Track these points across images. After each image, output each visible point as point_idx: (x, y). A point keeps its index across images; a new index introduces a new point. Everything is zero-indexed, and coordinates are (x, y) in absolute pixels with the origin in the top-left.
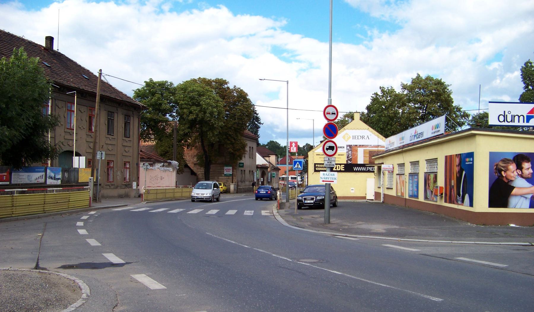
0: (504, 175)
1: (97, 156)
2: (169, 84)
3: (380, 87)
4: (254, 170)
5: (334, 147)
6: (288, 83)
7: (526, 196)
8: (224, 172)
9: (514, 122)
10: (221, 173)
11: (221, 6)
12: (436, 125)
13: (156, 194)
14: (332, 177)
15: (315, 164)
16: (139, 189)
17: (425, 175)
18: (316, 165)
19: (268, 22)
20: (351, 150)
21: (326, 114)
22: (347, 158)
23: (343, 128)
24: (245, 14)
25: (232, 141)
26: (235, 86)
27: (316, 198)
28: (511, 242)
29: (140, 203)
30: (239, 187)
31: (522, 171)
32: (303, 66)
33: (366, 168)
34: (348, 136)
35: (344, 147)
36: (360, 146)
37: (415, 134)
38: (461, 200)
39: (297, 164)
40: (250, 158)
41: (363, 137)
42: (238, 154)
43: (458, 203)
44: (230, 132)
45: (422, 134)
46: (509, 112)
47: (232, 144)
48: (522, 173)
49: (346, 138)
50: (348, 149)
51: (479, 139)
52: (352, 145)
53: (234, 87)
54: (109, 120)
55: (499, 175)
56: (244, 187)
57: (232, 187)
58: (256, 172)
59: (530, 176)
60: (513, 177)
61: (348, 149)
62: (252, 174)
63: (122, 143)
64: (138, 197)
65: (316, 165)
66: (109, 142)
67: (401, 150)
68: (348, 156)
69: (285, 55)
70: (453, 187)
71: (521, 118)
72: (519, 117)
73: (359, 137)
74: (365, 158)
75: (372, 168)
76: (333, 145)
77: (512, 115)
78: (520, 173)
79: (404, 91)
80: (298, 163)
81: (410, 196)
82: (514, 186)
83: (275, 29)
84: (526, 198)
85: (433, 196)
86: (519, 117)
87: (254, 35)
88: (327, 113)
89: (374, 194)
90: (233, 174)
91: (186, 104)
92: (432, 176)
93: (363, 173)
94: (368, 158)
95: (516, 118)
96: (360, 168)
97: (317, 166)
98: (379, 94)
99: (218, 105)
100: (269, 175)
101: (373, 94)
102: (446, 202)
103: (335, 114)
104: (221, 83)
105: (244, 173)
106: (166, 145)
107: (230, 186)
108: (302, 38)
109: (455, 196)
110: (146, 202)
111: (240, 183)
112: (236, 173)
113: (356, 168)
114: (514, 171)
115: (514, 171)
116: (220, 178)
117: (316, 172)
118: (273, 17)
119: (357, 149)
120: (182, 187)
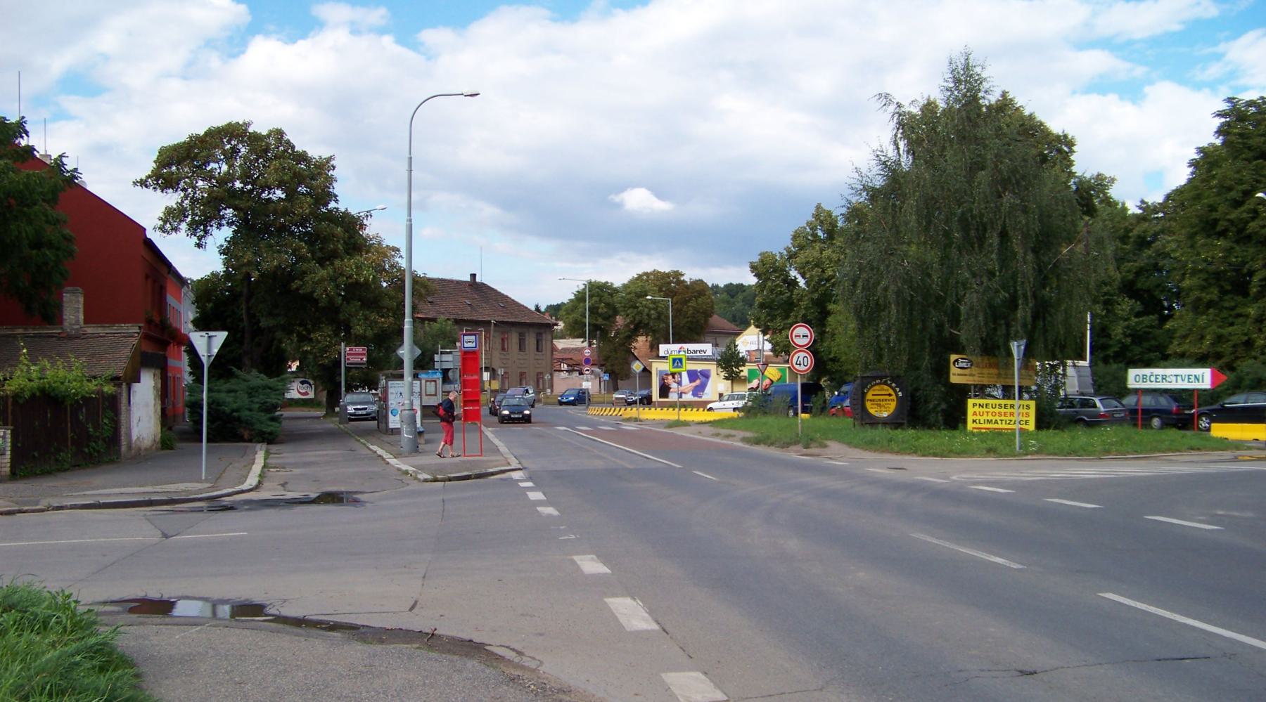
21: (794, 337)
54: (520, 339)
66: (521, 357)
88: (796, 336)
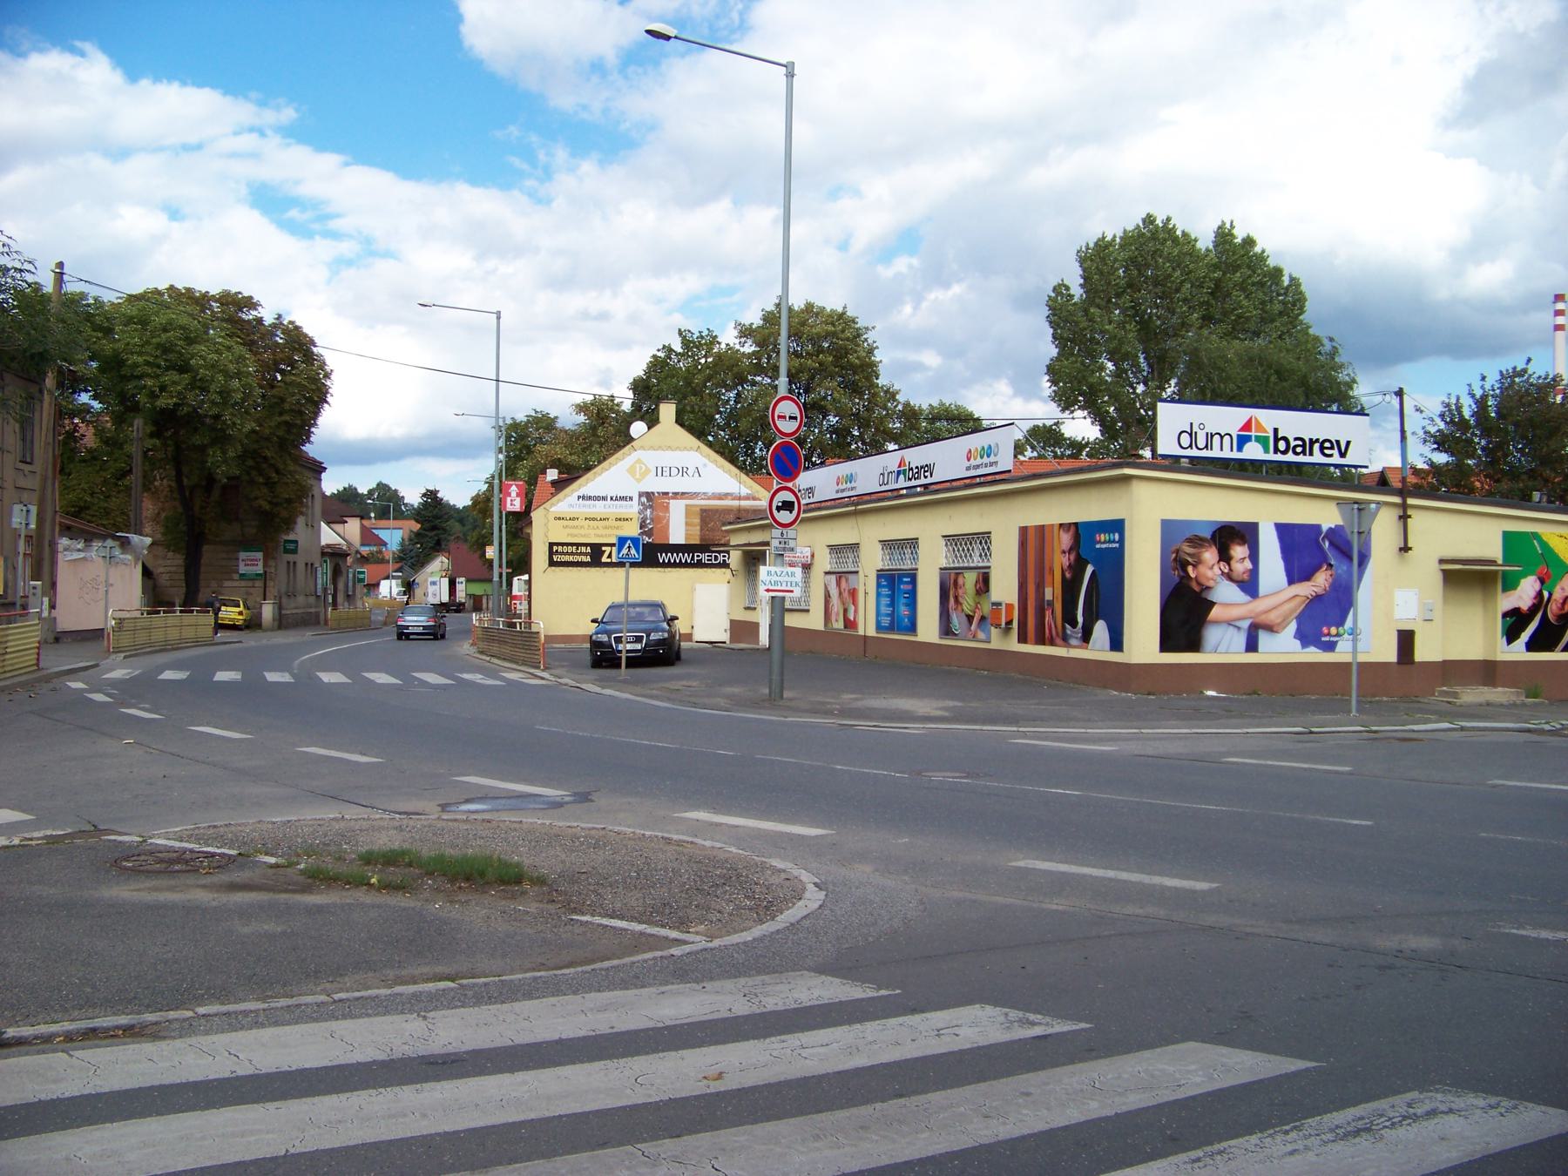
0: (1193, 575)
1: (14, 520)
2: (91, 301)
3: (680, 330)
4: (316, 560)
5: (794, 502)
6: (499, 318)
7: (1238, 624)
8: (238, 566)
9: (1211, 449)
11: (87, 47)
12: (983, 448)
13: (132, 632)
14: (790, 579)
15: (551, 545)
16: (55, 618)
17: (941, 574)
18: (555, 548)
19: (242, 111)
20: (651, 507)
22: (641, 529)
23: (629, 446)
24: (165, 81)
25: (269, 478)
26: (279, 317)
27: (648, 636)
28: (1258, 727)
29: (107, 658)
30: (283, 612)
31: (1229, 565)
32: (347, 248)
33: (693, 556)
34: (643, 466)
35: (631, 499)
36: (676, 495)
37: (900, 466)
38: (1080, 635)
39: (627, 545)
40: (307, 525)
41: (683, 471)
42: (284, 514)
43: (1069, 644)
44: (267, 451)
45: (927, 469)
46: (1202, 427)
47: (270, 484)
48: (1230, 569)
49: (638, 474)
50: (643, 504)
51: (1141, 491)
52: (653, 493)
53: (277, 319)
55: (1182, 574)
56: (294, 611)
57: (268, 611)
58: (321, 566)
59: (1246, 577)
60: (1212, 579)
61: (643, 504)
62: (312, 572)
63: (15, 481)
64: (52, 641)
65: (555, 548)
67: (854, 508)
68: (644, 522)
69: (294, 213)
70: (1051, 604)
71: (1226, 439)
72: (1222, 437)
73: (674, 471)
74: (690, 528)
75: (708, 556)
76: (791, 498)
77: (1207, 434)
78: (1226, 571)
79: (745, 342)
80: (629, 542)
81: (879, 628)
82: (1214, 601)
83: (261, 132)
84: (1239, 628)
85: (973, 627)
86: (1222, 437)
87: (199, 147)
88: (779, 417)
89: (727, 626)
90: (265, 572)
91: (147, 363)
92: (970, 579)
93: (682, 570)
94: (698, 528)
95: (1217, 438)
96: (675, 554)
97: (557, 551)
98: (676, 350)
99: (242, 370)
100: (351, 576)
101: (659, 350)
102: (1023, 639)
103: (795, 418)
104: (235, 304)
105: (294, 570)
106: (83, 486)
107: (261, 607)
108: (347, 164)
109: (1056, 627)
110: (123, 655)
111: (284, 600)
112: (276, 570)
113: (664, 555)
114: (1213, 565)
115: (1213, 565)
116: (227, 584)
117: (553, 568)
118: (254, 95)
119: (669, 503)
120: (181, 611)
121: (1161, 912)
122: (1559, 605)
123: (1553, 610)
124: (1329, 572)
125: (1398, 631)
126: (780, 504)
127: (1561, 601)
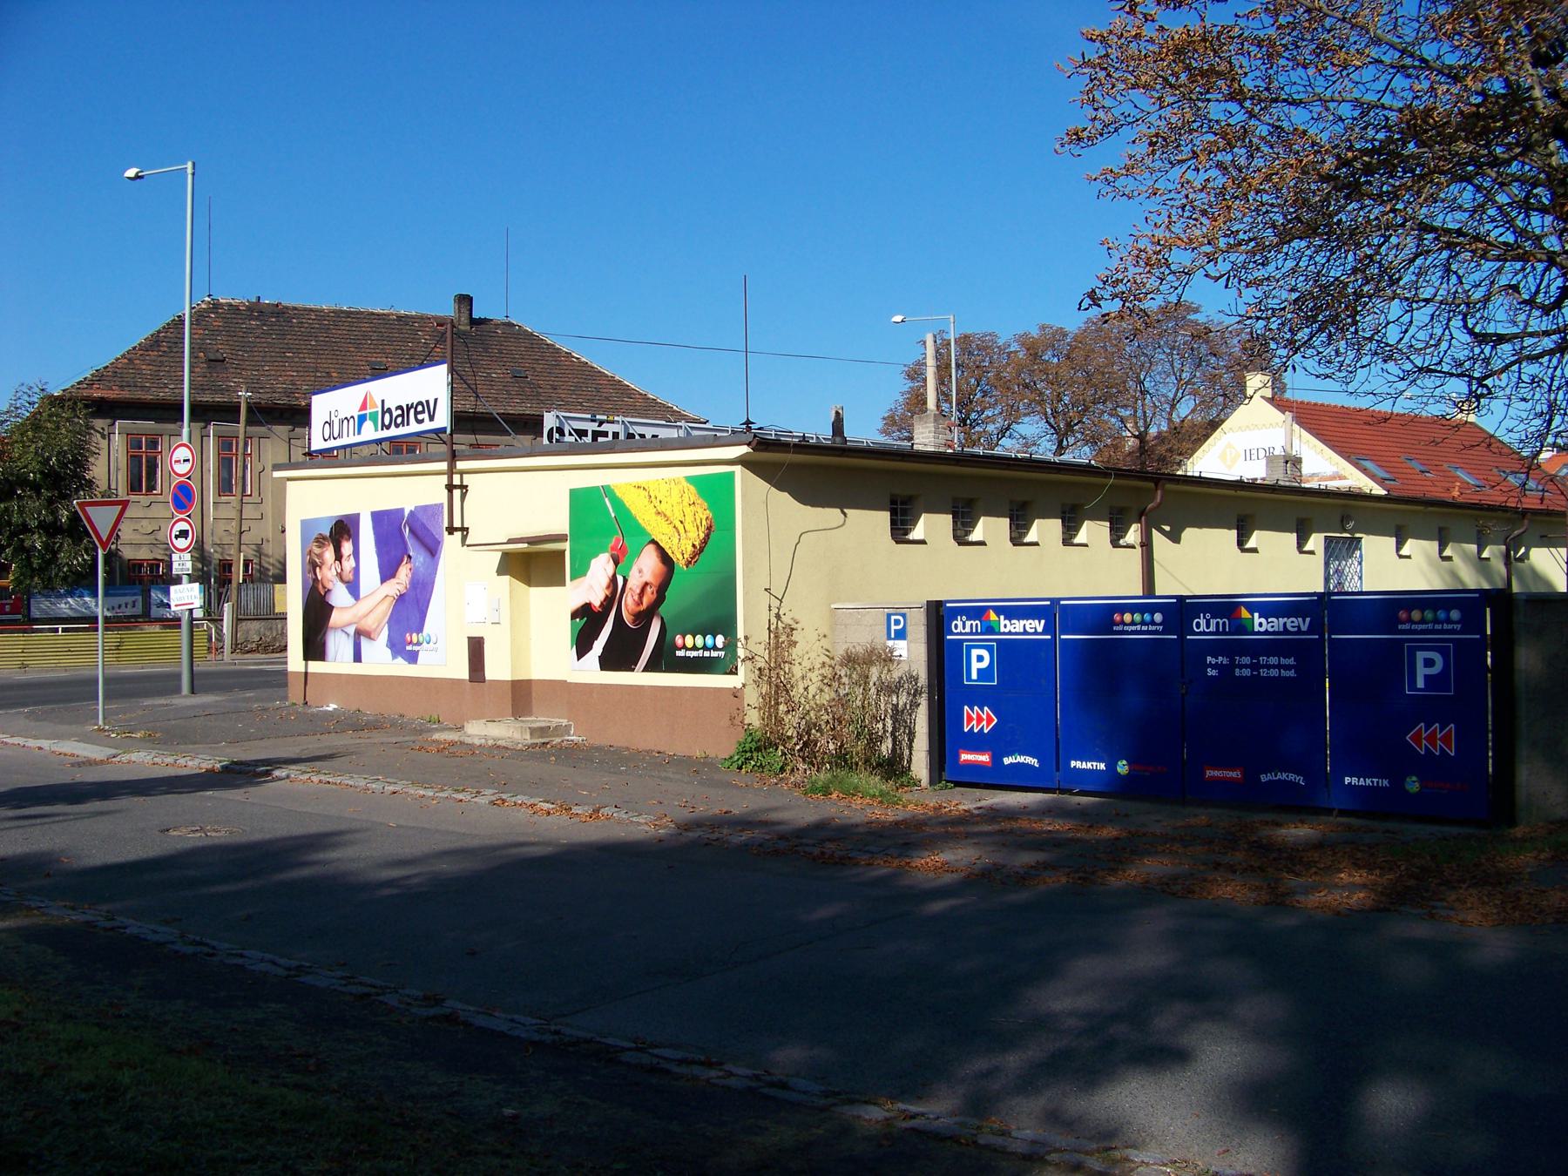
10: (81, 596)
14: (189, 594)
72: (348, 421)
88: (176, 462)
95: (346, 421)
103: (188, 460)
121: (12, 923)
122: (636, 598)
123: (629, 604)
124: (409, 566)
125: (469, 638)
126: (178, 533)
127: (638, 591)
